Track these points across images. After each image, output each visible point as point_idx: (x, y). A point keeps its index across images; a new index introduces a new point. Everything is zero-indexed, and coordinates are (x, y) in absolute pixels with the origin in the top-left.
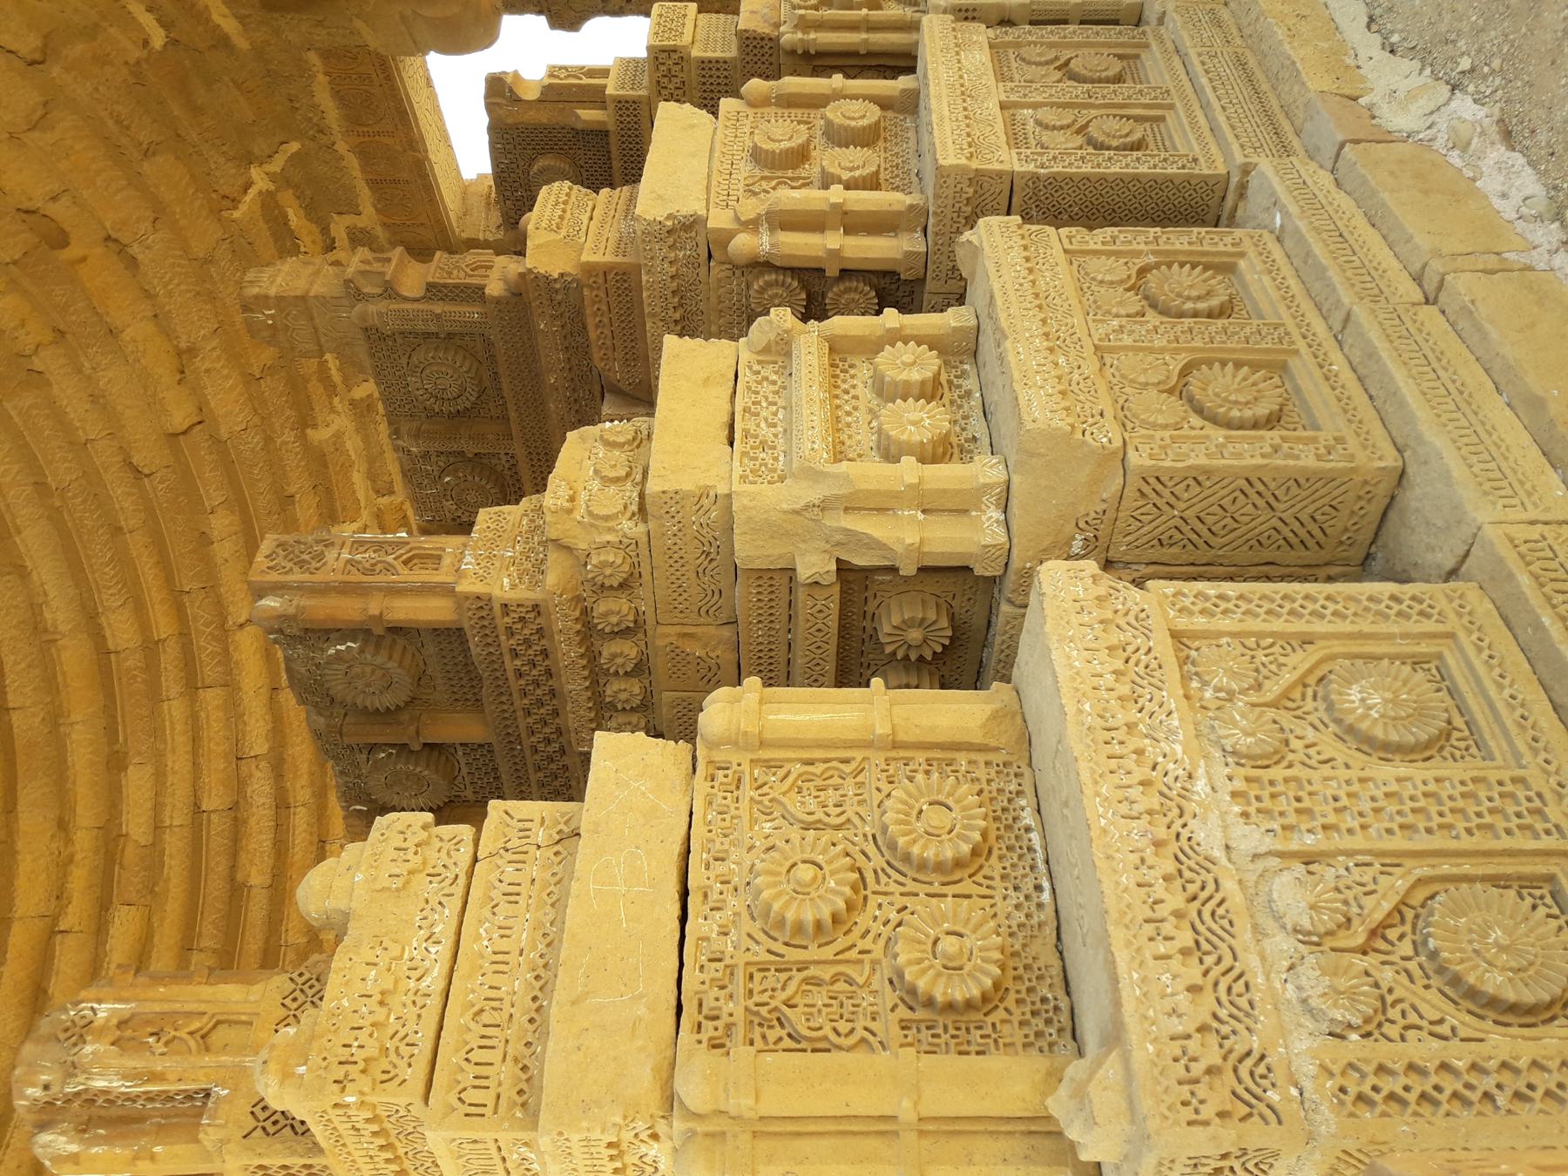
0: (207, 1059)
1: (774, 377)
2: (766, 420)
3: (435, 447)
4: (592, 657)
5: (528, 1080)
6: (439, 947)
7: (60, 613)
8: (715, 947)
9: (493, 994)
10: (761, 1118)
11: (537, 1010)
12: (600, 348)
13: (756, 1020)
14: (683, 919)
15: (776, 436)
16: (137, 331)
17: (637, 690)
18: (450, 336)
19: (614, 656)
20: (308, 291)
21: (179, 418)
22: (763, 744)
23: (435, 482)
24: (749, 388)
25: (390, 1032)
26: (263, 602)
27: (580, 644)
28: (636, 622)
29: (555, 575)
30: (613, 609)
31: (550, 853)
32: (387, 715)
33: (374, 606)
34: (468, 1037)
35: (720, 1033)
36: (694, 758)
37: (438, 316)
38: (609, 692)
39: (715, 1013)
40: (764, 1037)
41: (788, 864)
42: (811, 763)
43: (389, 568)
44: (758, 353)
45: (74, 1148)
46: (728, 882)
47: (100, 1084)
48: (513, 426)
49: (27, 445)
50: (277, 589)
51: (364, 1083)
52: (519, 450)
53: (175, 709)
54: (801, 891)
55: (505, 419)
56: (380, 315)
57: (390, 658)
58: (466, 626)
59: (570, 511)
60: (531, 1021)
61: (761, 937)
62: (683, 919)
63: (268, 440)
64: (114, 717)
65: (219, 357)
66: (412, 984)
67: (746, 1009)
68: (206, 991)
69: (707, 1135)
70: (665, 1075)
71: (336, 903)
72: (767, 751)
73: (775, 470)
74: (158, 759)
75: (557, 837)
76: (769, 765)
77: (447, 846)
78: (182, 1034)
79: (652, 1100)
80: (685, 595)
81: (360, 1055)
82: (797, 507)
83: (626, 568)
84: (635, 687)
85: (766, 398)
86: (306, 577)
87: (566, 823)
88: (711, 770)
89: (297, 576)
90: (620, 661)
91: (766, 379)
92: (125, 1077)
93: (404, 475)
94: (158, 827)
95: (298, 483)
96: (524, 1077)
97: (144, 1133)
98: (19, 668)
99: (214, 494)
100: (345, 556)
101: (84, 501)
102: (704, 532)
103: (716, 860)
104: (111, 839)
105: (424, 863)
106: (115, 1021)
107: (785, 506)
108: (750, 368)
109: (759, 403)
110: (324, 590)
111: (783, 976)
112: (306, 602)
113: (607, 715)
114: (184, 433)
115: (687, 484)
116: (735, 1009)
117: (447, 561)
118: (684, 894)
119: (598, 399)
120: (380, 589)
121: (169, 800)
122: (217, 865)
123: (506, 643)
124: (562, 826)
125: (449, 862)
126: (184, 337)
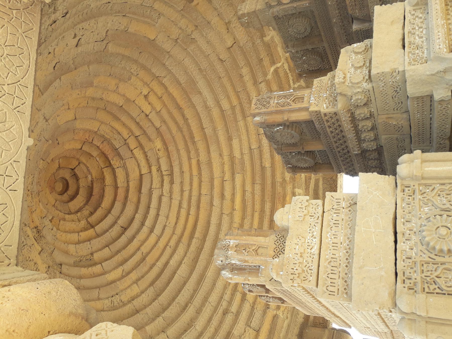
0: (258, 258)
1: (421, 15)
2: (418, 35)
3: (299, 49)
4: (356, 127)
5: (347, 285)
6: (316, 240)
7: (211, 103)
8: (408, 254)
9: (334, 256)
10: (429, 317)
11: (348, 263)
12: (351, 6)
13: (425, 281)
14: (396, 242)
15: (423, 42)
16: (215, 20)
17: (372, 135)
18: (300, 13)
19: (363, 126)
20: (255, 9)
21: (229, 43)
22: (423, 178)
23: (300, 59)
24: (410, 22)
25: (305, 265)
26: (255, 119)
27: (351, 124)
28: (370, 115)
29: (340, 105)
30: (361, 112)
31: (347, 210)
32: (294, 145)
33: (286, 117)
34: (328, 270)
35: (412, 285)
36: (396, 183)
37: (295, 8)
38: (362, 136)
39: (410, 277)
40: (428, 287)
41: (436, 227)
42: (443, 184)
43: (289, 104)
44: (414, 6)
45: (230, 276)
46: (412, 230)
47: (233, 262)
48: (323, 37)
49: (195, 59)
50: (259, 114)
51: (299, 280)
52: (326, 45)
53: (241, 124)
54: (441, 238)
55: (320, 35)
56: (278, 12)
57: (292, 130)
58: (314, 120)
59: (344, 83)
60: (347, 266)
61: (426, 252)
62: (396, 242)
63: (253, 43)
64: (227, 127)
65: (237, 22)
66: (309, 251)
67: (421, 277)
68: (255, 238)
69: (409, 319)
70: (393, 295)
71: (285, 223)
72: (425, 181)
73: (423, 58)
74: (239, 136)
75: (349, 205)
76: (426, 185)
77: (315, 207)
78: (251, 250)
79: (389, 304)
80: (388, 105)
81: (296, 272)
82: (433, 73)
83: (366, 99)
84: (372, 135)
85: (418, 25)
86: (266, 110)
87: (352, 200)
88: (403, 188)
89: (263, 110)
90: (365, 127)
91: (417, 16)
92: (239, 261)
93: (291, 59)
94: (242, 154)
95: (263, 55)
96: (346, 284)
97: (246, 274)
98: (204, 118)
99: (242, 63)
100: (276, 101)
101: (211, 71)
102: (394, 84)
103: (407, 221)
104: (232, 158)
105: (308, 212)
106: (235, 245)
107: (428, 73)
108: (410, 13)
109: (414, 29)
110: (271, 113)
111: (435, 266)
112: (266, 117)
113: (363, 142)
114: (231, 47)
115: (387, 69)
116: (417, 276)
117: (306, 99)
118: (396, 233)
119: (351, 23)
120: (287, 111)
121: (243, 147)
122: (257, 162)
123: (327, 124)
124: (351, 201)
125: (316, 212)
126: (227, 19)
